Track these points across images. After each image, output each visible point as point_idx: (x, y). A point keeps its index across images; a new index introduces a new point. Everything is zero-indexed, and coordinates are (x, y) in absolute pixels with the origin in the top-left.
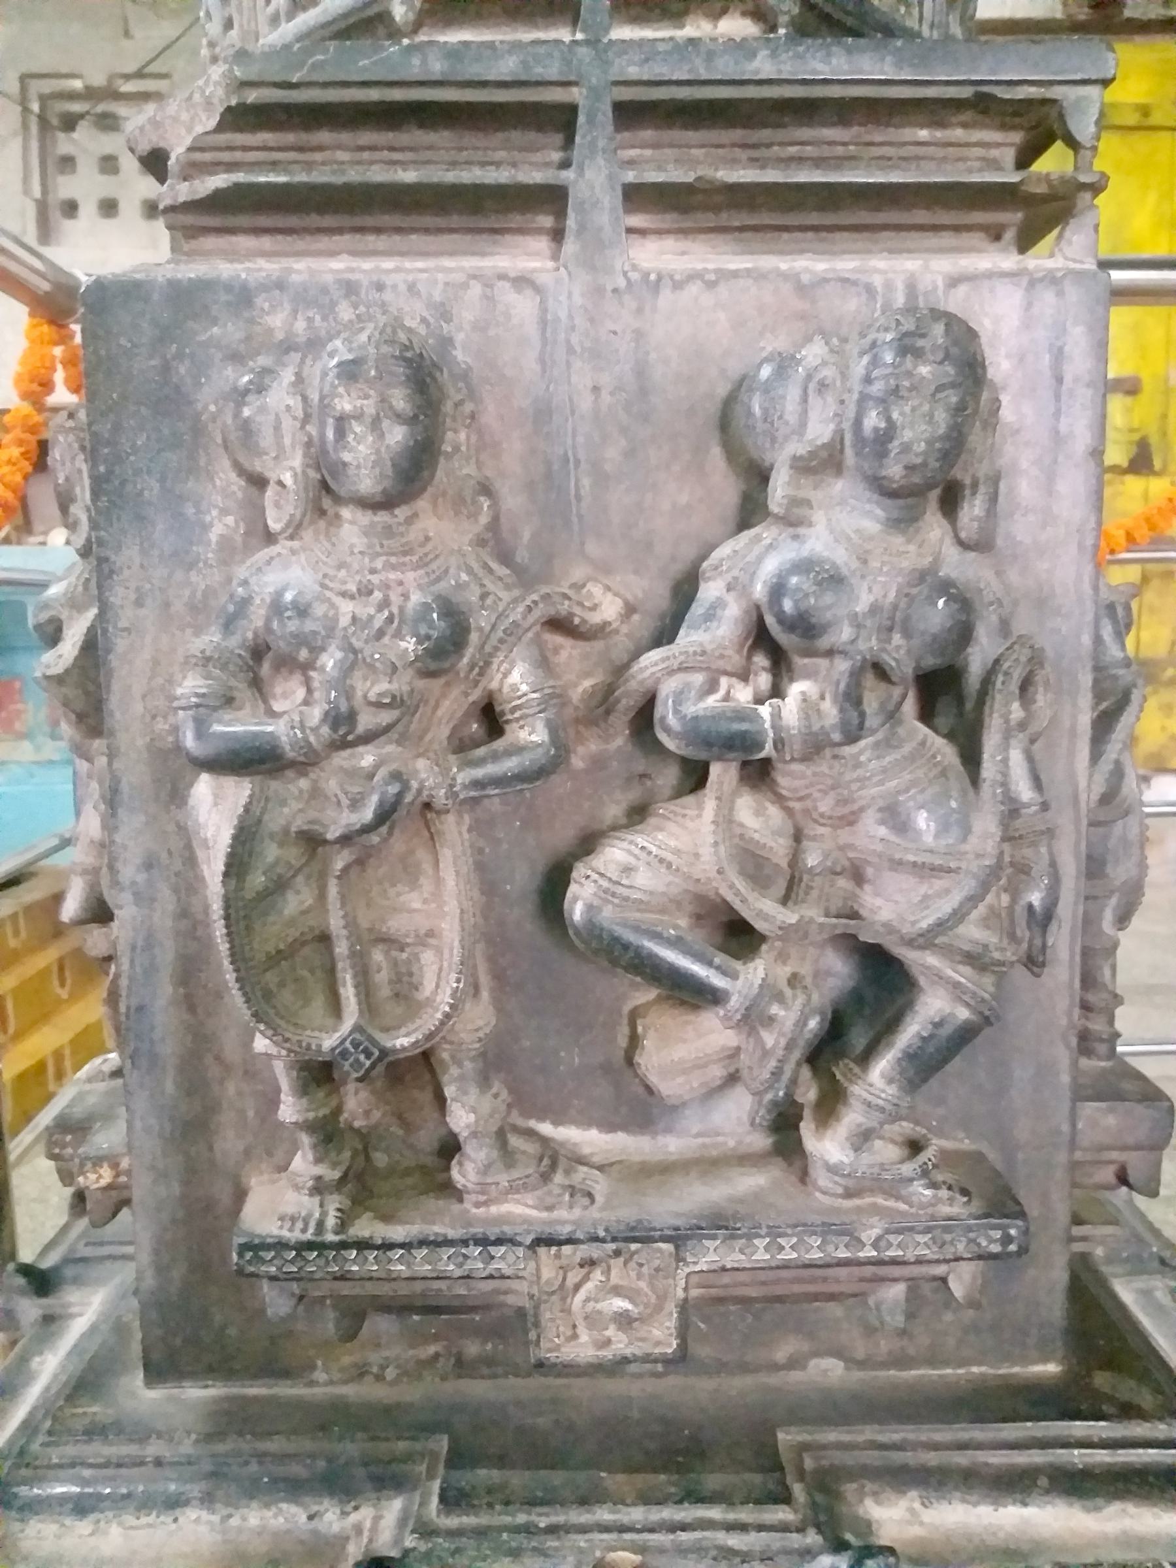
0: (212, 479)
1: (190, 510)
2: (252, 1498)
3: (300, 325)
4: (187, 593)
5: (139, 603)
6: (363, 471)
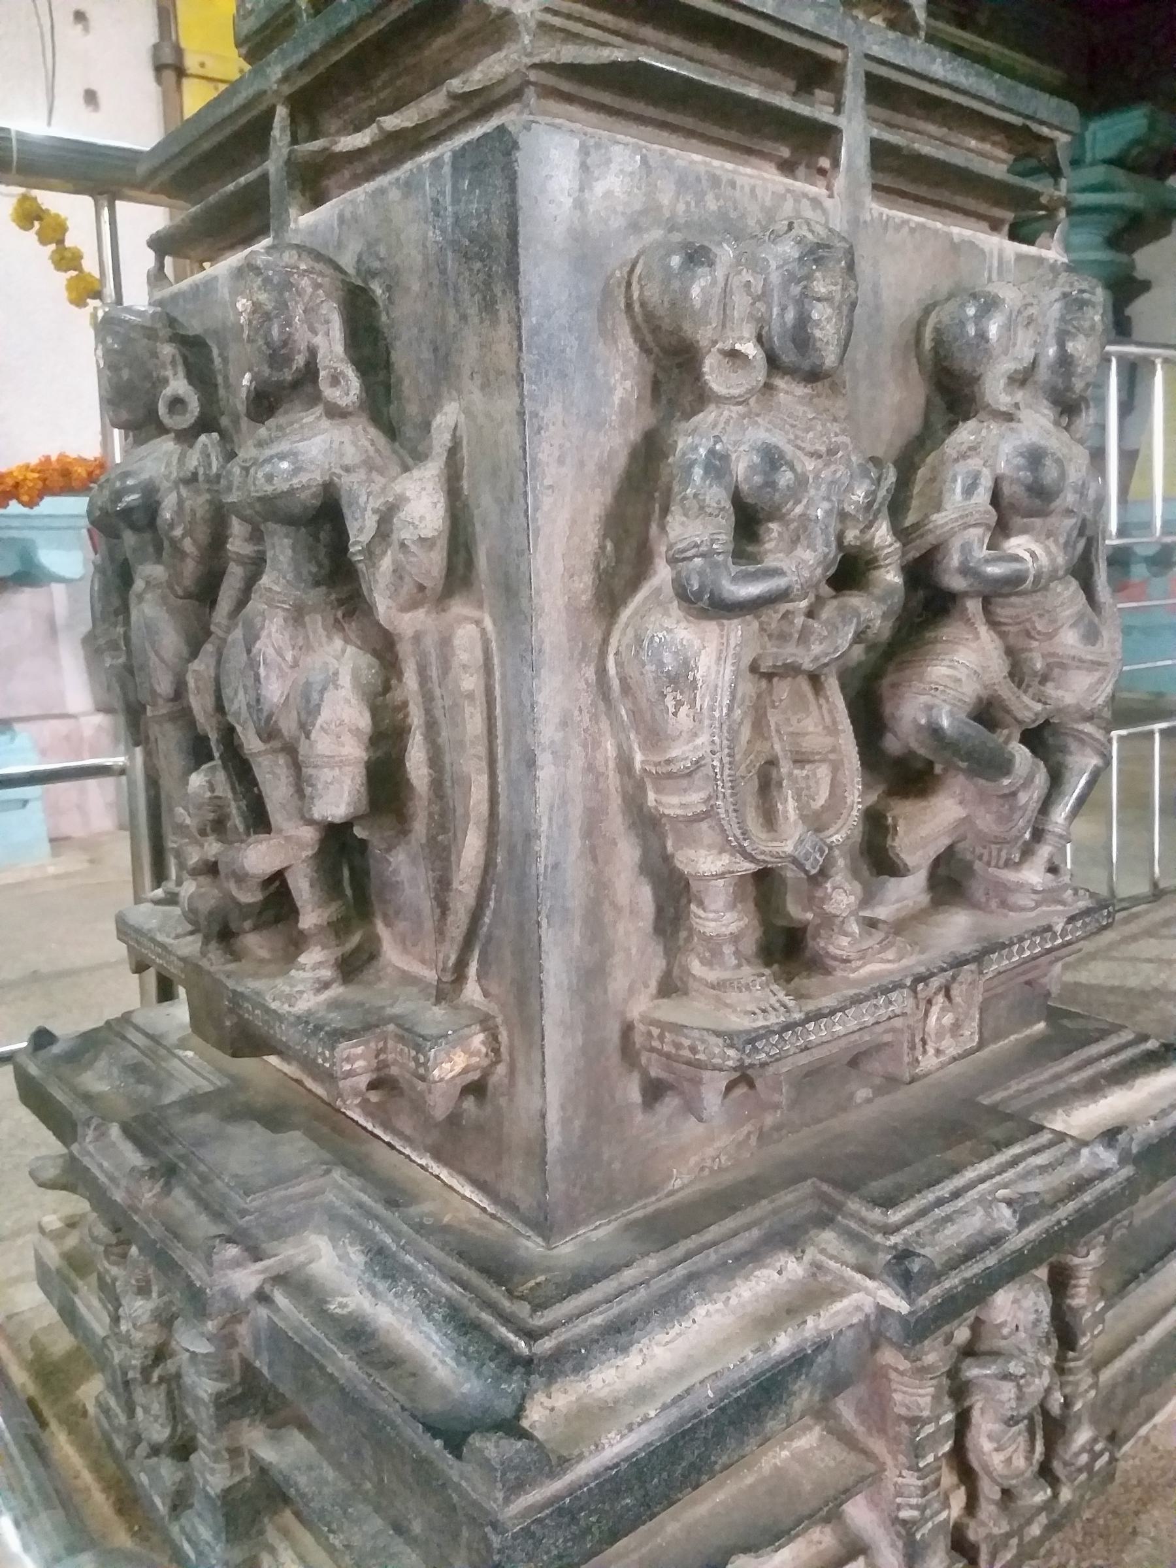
0: (616, 342)
1: (600, 372)
2: (733, 1279)
3: (681, 207)
4: (597, 454)
5: (561, 461)
6: (831, 348)
